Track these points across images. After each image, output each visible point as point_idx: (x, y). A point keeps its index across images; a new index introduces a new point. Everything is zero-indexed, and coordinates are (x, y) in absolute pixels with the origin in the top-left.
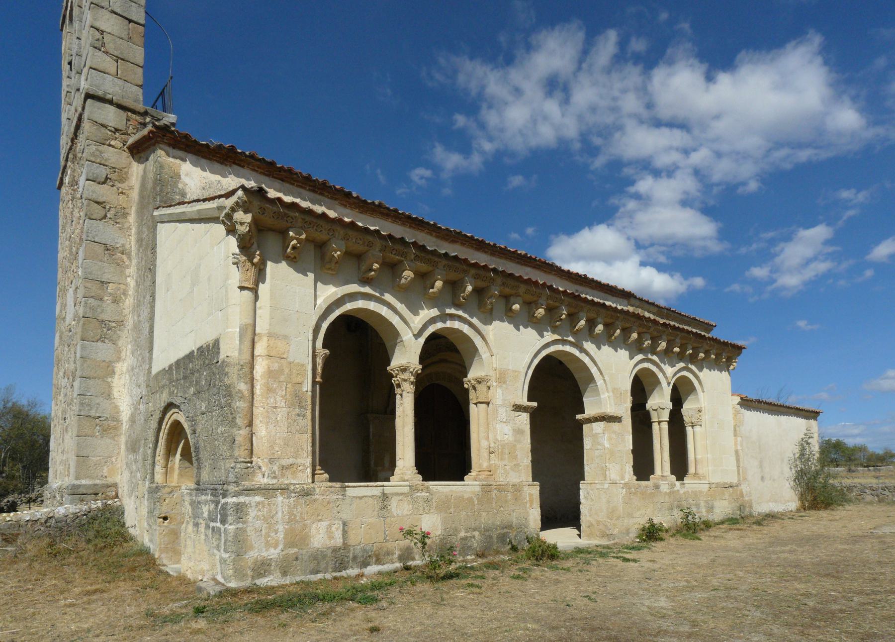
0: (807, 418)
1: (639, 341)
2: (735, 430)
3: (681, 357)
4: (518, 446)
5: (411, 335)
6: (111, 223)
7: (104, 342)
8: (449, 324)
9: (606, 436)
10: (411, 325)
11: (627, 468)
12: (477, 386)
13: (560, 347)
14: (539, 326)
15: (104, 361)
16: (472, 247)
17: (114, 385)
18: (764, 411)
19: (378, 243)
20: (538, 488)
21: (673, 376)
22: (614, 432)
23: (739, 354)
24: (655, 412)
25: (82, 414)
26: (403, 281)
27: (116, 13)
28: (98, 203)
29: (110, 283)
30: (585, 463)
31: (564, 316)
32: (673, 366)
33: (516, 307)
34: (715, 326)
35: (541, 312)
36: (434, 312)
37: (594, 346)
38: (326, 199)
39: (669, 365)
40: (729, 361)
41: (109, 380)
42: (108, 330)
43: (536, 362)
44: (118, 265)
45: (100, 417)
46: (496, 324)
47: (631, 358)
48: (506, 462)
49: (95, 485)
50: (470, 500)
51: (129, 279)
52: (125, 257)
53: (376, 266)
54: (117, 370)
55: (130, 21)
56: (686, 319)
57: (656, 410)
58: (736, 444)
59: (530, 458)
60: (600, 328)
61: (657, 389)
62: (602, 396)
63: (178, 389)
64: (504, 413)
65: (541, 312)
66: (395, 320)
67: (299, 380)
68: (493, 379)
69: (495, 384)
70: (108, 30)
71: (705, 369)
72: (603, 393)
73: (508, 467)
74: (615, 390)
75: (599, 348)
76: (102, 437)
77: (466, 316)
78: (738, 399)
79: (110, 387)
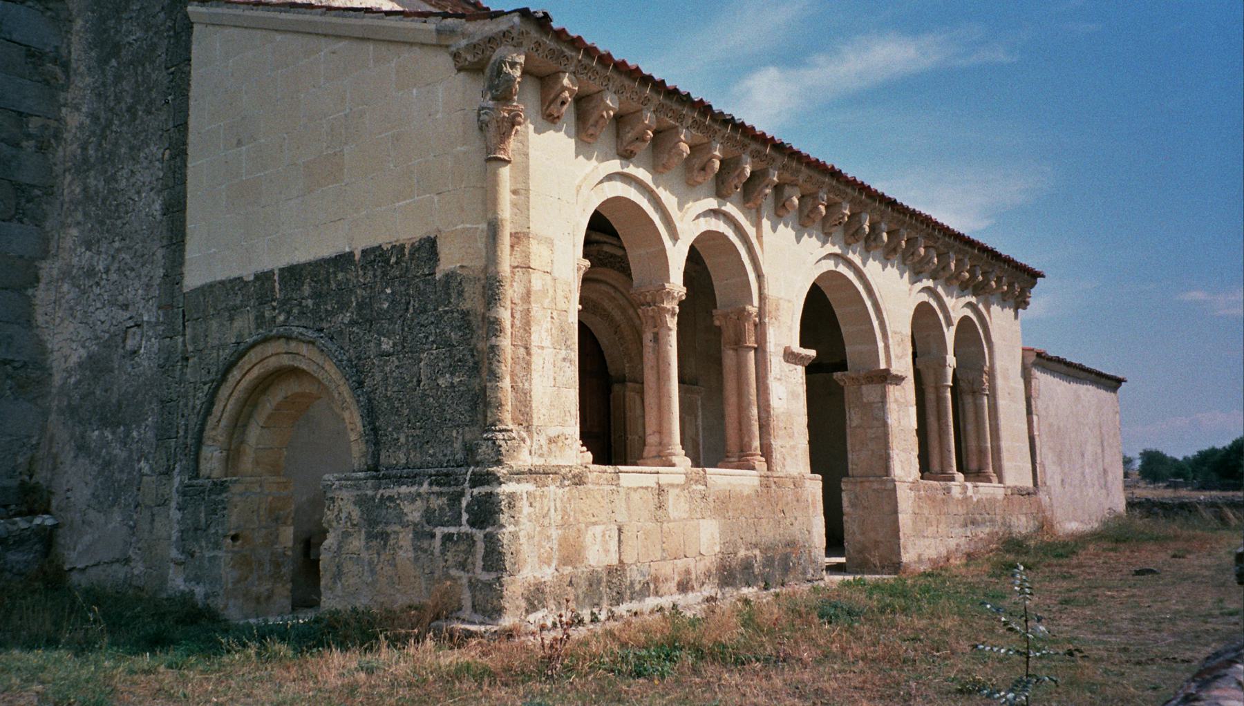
6: (37, 10)
7: (22, 222)
15: (21, 257)
20: (821, 484)
29: (32, 115)
42: (28, 201)
44: (48, 83)
45: (13, 361)
50: (748, 496)
51: (64, 110)
54: (43, 274)
63: (289, 313)
67: (564, 307)
76: (16, 399)
79: (31, 305)
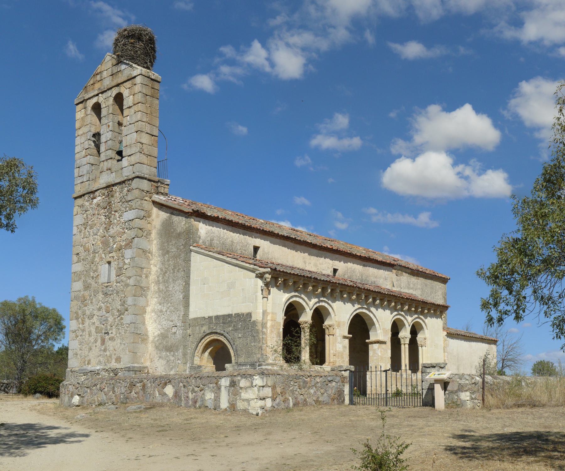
0: (489, 343)
1: (395, 306)
2: (444, 349)
3: (416, 312)
4: (344, 353)
5: (309, 309)
8: (321, 304)
9: (379, 350)
10: (310, 306)
11: (388, 365)
12: (329, 328)
13: (361, 310)
14: (353, 302)
16: (310, 247)
17: (146, 318)
18: (461, 339)
19: (302, 278)
21: (412, 322)
22: (383, 349)
23: (447, 310)
24: (403, 339)
25: (135, 332)
26: (308, 290)
27: (148, 133)
28: (140, 229)
30: (370, 362)
31: (363, 298)
32: (412, 317)
33: (345, 296)
34: (449, 279)
35: (354, 297)
36: (316, 300)
37: (375, 309)
38: (249, 232)
39: (410, 316)
40: (442, 313)
41: (144, 316)
43: (351, 317)
46: (337, 302)
47: (391, 314)
48: (340, 360)
49: (140, 367)
51: (151, 266)
52: (150, 255)
53: (301, 286)
54: (147, 311)
55: (153, 136)
56: (429, 275)
57: (403, 338)
58: (444, 357)
59: (348, 358)
60: (378, 302)
61: (404, 328)
62: (378, 332)
64: (339, 339)
65: (354, 297)
66: (304, 304)
68: (335, 325)
69: (336, 327)
70: (145, 143)
71: (428, 317)
72: (379, 331)
73: (340, 362)
74: (384, 329)
75: (377, 310)
77: (327, 300)
78: (445, 333)
79: (144, 319)
